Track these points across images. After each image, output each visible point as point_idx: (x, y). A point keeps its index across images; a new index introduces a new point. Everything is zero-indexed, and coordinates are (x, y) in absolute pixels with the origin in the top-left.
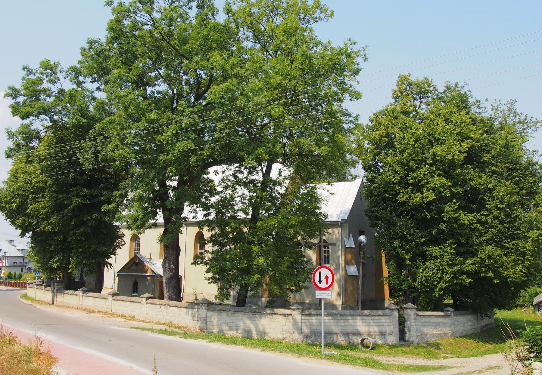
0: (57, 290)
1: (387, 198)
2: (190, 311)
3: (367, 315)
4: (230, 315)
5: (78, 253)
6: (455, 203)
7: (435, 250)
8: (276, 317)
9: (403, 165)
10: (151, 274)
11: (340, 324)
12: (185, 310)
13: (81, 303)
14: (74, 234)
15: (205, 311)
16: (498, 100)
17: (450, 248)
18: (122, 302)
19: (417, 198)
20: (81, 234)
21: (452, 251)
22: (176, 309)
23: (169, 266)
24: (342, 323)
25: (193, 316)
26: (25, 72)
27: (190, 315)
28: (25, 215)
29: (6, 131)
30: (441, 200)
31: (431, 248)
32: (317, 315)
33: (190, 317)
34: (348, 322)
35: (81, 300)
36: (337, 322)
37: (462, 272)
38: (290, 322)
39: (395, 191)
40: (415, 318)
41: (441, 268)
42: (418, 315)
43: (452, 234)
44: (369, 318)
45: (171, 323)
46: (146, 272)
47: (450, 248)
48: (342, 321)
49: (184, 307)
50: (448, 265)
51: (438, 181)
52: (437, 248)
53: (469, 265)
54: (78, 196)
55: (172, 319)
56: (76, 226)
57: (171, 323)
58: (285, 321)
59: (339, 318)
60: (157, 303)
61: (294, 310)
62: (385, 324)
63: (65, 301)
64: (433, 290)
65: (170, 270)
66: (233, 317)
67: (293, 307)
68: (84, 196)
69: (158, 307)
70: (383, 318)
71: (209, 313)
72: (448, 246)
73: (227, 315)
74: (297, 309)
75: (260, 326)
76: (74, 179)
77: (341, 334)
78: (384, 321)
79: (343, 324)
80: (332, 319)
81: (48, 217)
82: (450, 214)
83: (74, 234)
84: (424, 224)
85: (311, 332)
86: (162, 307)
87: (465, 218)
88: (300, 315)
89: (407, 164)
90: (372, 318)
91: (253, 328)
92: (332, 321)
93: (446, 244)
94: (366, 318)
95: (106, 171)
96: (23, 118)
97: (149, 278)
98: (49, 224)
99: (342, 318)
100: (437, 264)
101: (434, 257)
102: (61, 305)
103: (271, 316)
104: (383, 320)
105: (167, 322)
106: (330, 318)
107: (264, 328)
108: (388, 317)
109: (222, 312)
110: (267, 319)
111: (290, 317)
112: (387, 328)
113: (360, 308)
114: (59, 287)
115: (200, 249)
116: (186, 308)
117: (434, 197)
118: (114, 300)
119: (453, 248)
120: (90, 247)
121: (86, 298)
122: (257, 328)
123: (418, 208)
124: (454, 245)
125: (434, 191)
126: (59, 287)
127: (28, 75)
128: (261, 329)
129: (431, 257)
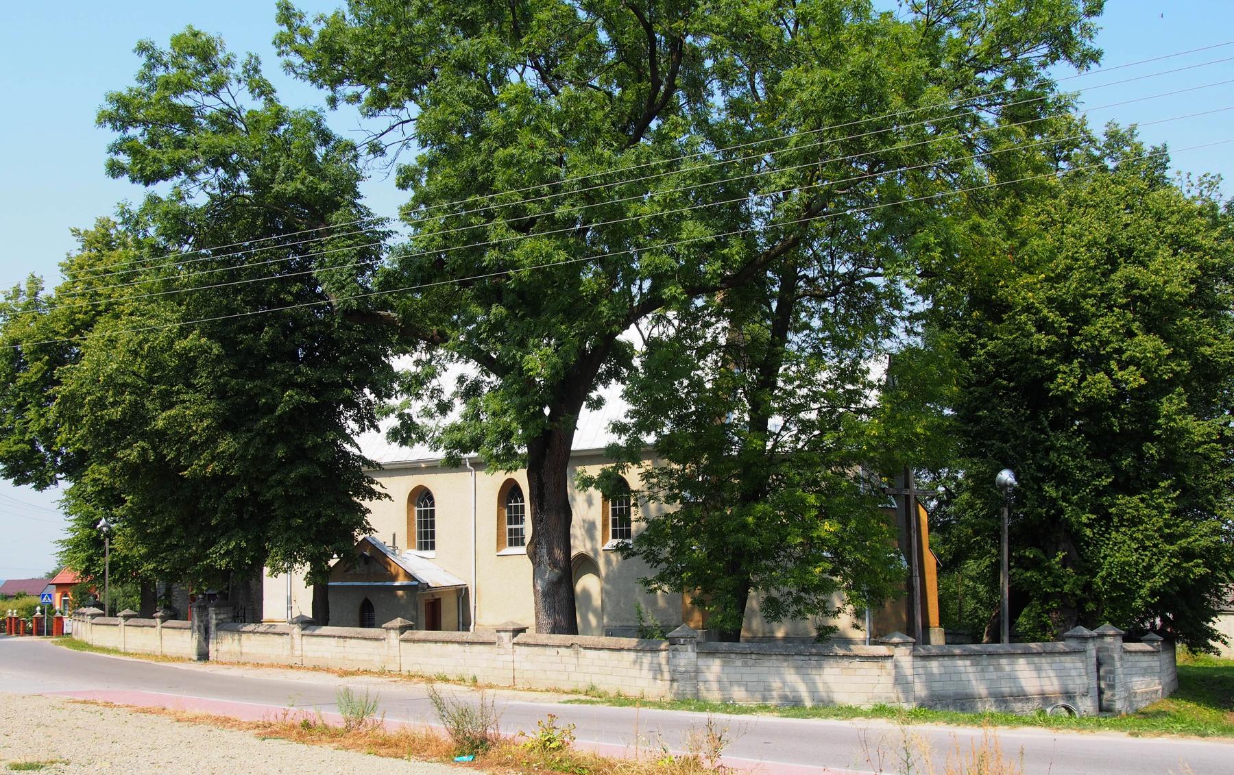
0: (217, 625)
1: (1004, 387)
2: (647, 658)
3: (1039, 654)
4: (751, 662)
5: (289, 528)
6: (1180, 395)
7: (1128, 503)
8: (856, 663)
9: (1061, 307)
10: (405, 583)
11: (988, 676)
12: (632, 655)
13: (298, 653)
14: (280, 483)
15: (693, 655)
16: (1184, 175)
17: (1165, 494)
18: (432, 645)
19: (1100, 384)
20: (305, 480)
21: (1174, 505)
22: (605, 654)
23: (550, 553)
24: (992, 674)
25: (657, 671)
26: (144, 59)
27: (646, 666)
28: (144, 436)
29: (119, 210)
30: (1157, 388)
31: (1121, 500)
32: (943, 656)
33: (647, 674)
34: (1002, 670)
35: (297, 647)
36: (983, 671)
37: (1188, 554)
38: (889, 675)
39: (1042, 368)
40: (1121, 659)
41: (1147, 543)
42: (1126, 652)
43: (1170, 465)
44: (1043, 660)
45: (593, 688)
46: (394, 578)
47: (1165, 494)
48: (991, 668)
49: (629, 650)
50: (1161, 536)
51: (1148, 344)
52: (1136, 499)
53: (1201, 536)
54: (288, 384)
55: (596, 680)
56: (291, 461)
57: (593, 688)
58: (878, 672)
59: (985, 661)
60: (545, 642)
61: (896, 645)
62: (1073, 673)
63: (245, 650)
64: (1131, 594)
65: (554, 564)
66: (758, 669)
67: (896, 640)
68: (301, 387)
69: (549, 651)
70: (1068, 658)
71: (701, 662)
72: (1161, 495)
73: (745, 665)
74: (903, 644)
75: (820, 687)
76: (272, 344)
77: (992, 700)
78: (1071, 665)
79: (994, 676)
80: (972, 665)
81: (211, 441)
82: (1174, 420)
83: (280, 483)
84: (1104, 445)
85: (932, 696)
86: (562, 651)
87: (1198, 428)
88: (910, 658)
89: (1076, 306)
90: (1049, 660)
91: (803, 691)
92: (970, 669)
93: (1156, 491)
94: (1036, 659)
95: (382, 316)
96: (147, 184)
97: (400, 593)
98: (214, 459)
99: (994, 662)
100: (1139, 536)
101: (1128, 520)
102: (235, 659)
103: (845, 663)
104: (1068, 662)
105: (582, 686)
106: (968, 662)
107: (829, 691)
108: (1075, 658)
109: (733, 656)
110: (837, 671)
111: (889, 664)
112: (1078, 681)
113: (1006, 638)
114: (222, 616)
115: (510, 523)
116: (636, 651)
117: (1143, 381)
118: (518, 644)
119: (1173, 499)
120: (319, 515)
121: (314, 639)
122: (813, 692)
123: (1094, 409)
124: (1175, 491)
125: (1138, 365)
126: (222, 616)
127: (151, 67)
128: (824, 695)
129: (1121, 520)
